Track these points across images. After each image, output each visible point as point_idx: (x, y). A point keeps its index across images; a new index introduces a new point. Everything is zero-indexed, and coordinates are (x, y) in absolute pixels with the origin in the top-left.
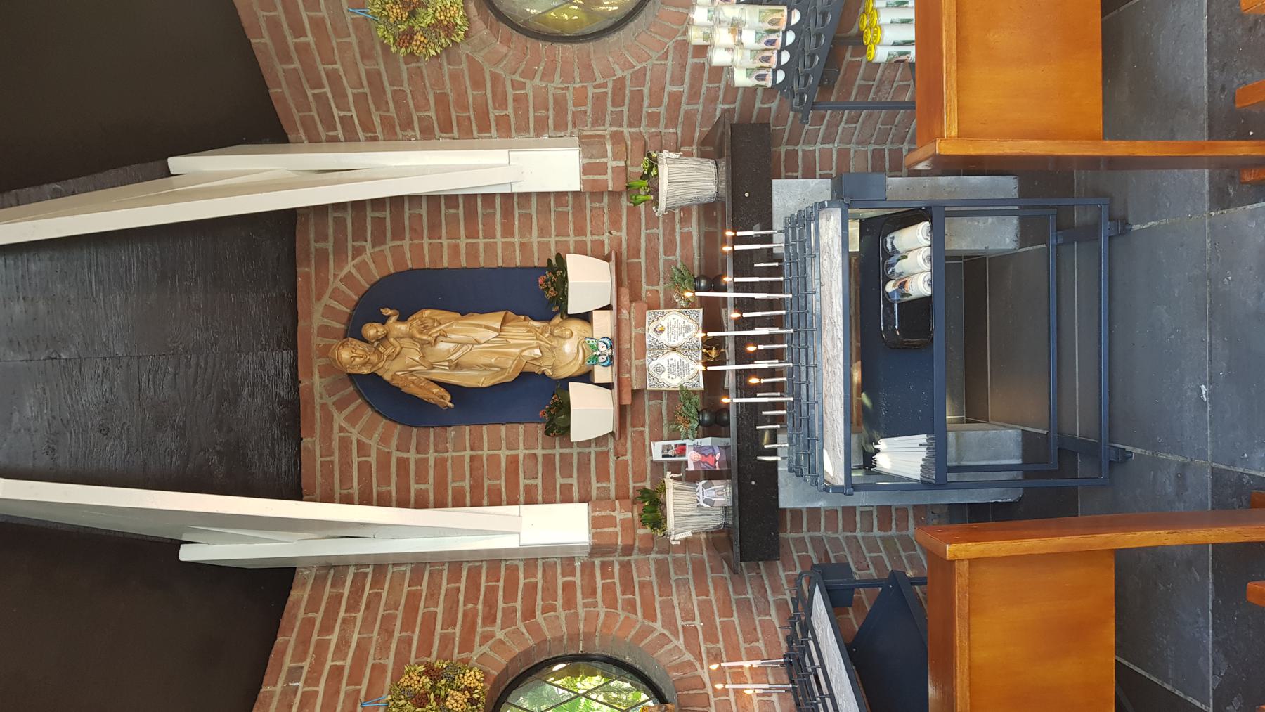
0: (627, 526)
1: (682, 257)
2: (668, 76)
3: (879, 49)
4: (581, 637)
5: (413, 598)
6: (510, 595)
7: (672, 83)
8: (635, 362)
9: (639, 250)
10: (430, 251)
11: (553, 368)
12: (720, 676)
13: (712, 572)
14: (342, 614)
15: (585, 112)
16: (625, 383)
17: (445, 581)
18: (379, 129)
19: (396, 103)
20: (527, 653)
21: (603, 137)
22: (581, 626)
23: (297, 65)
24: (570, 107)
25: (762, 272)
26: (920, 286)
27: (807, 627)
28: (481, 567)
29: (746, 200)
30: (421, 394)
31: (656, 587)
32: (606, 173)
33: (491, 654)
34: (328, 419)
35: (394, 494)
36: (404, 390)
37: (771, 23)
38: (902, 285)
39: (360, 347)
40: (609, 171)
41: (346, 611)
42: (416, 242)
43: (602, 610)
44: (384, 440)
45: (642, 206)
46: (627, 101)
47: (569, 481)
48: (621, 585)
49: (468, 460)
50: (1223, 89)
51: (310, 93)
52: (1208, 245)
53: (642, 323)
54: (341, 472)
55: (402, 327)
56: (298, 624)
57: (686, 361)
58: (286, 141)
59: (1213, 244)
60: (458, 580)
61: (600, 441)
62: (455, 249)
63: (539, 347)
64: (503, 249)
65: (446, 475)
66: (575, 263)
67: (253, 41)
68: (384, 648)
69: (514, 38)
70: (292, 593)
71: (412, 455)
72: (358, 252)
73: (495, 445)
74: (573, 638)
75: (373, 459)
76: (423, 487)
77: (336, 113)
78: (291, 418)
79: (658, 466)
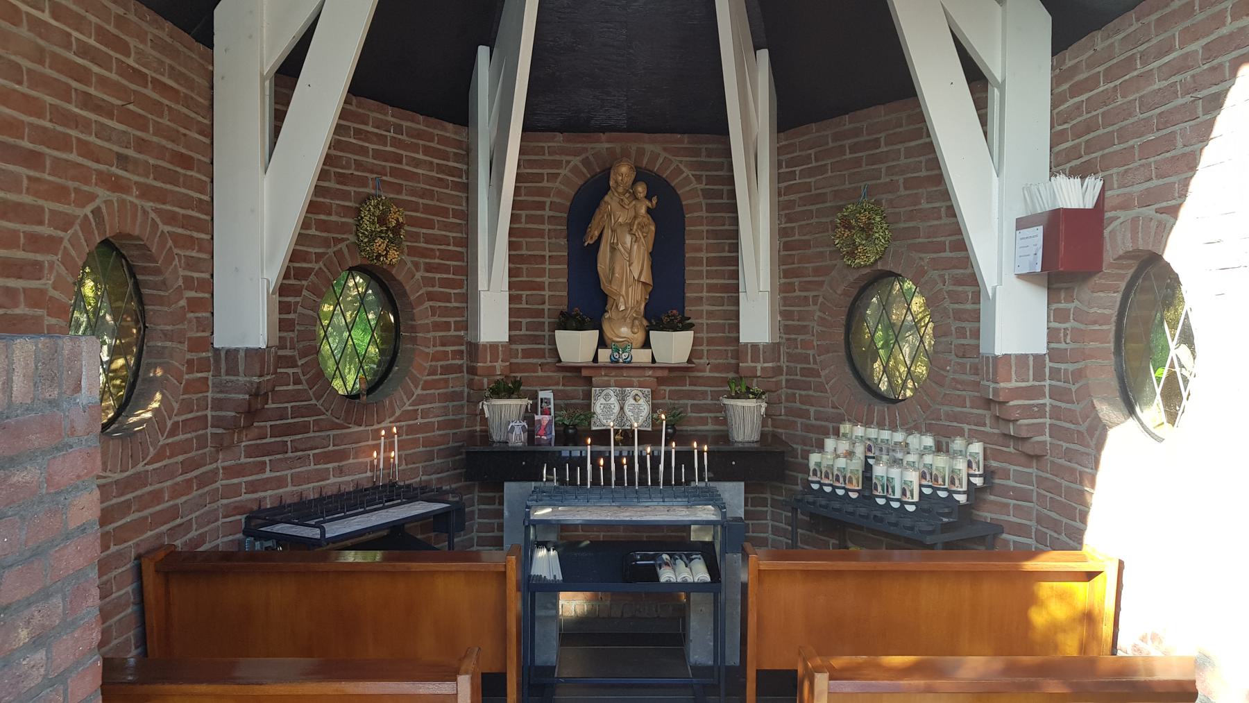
5: (443, 212)
8: (612, 380)
12: (389, 435)
14: (436, 161)
18: (786, 198)
20: (405, 294)
23: (831, 145)
24: (800, 337)
25: (678, 468)
26: (666, 575)
29: (730, 462)
30: (594, 222)
34: (576, 153)
38: (667, 564)
39: (629, 180)
43: (431, 350)
44: (559, 193)
45: (728, 388)
49: (543, 253)
51: (812, 152)
55: (643, 211)
58: (779, 131)
61: (555, 352)
62: (699, 249)
63: (626, 309)
64: (699, 284)
66: (688, 335)
68: (413, 192)
71: (547, 213)
72: (698, 178)
73: (553, 274)
74: (413, 329)
75: (545, 184)
76: (523, 220)
77: (798, 169)
78: (577, 125)
79: (534, 396)
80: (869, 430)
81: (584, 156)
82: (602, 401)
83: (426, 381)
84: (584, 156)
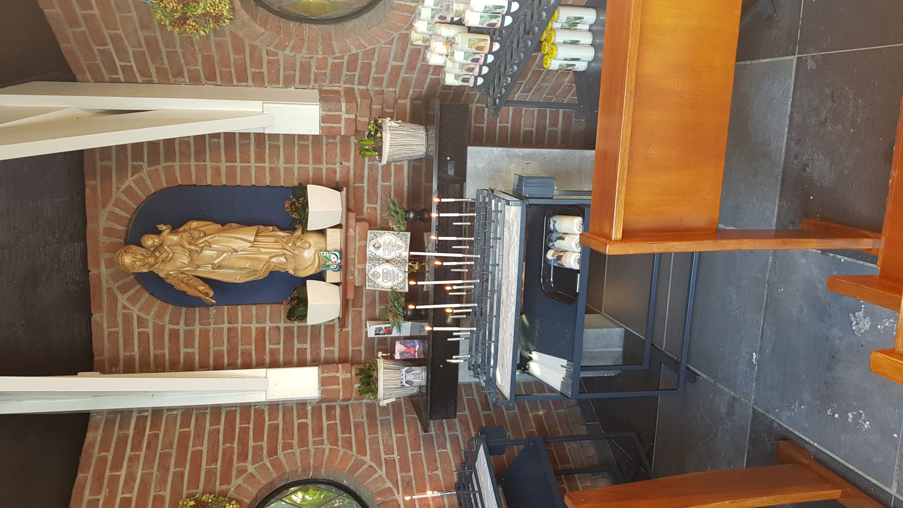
0: (347, 384)
1: (395, 183)
2: (392, 55)
3: (553, 62)
4: (312, 469)
5: (184, 437)
6: (258, 436)
7: (395, 59)
8: (358, 266)
9: (363, 177)
10: (196, 171)
11: (295, 270)
13: (407, 413)
15: (325, 74)
16: (350, 283)
17: (208, 424)
18: (154, 75)
19: (169, 60)
20: (271, 483)
21: (338, 92)
22: (312, 461)
23: (84, 28)
24: (313, 69)
26: (572, 261)
27: (473, 468)
28: (236, 411)
31: (366, 427)
32: (340, 123)
33: (245, 485)
34: (114, 300)
35: (167, 355)
36: (177, 287)
37: (478, 48)
40: (343, 121)
41: (132, 450)
42: (185, 163)
43: (327, 447)
44: (160, 316)
46: (358, 69)
47: (304, 346)
48: (341, 425)
49: (226, 331)
50: (796, 157)
52: (770, 261)
53: (365, 238)
54: (125, 340)
55: (175, 238)
56: (94, 462)
57: (396, 270)
59: (774, 262)
60: (218, 423)
61: (329, 326)
62: (217, 170)
64: (255, 172)
65: (209, 342)
66: (311, 188)
67: (45, 11)
68: (162, 482)
69: (270, 20)
70: (88, 435)
71: (182, 327)
72: (136, 170)
73: (247, 319)
74: (306, 470)
75: (150, 330)
76: (190, 350)
77: (118, 63)
78: (82, 298)
79: (370, 341)
80: (422, 16)
81: (117, 292)
82: (380, 279)
83: (358, 452)
84: (117, 292)
